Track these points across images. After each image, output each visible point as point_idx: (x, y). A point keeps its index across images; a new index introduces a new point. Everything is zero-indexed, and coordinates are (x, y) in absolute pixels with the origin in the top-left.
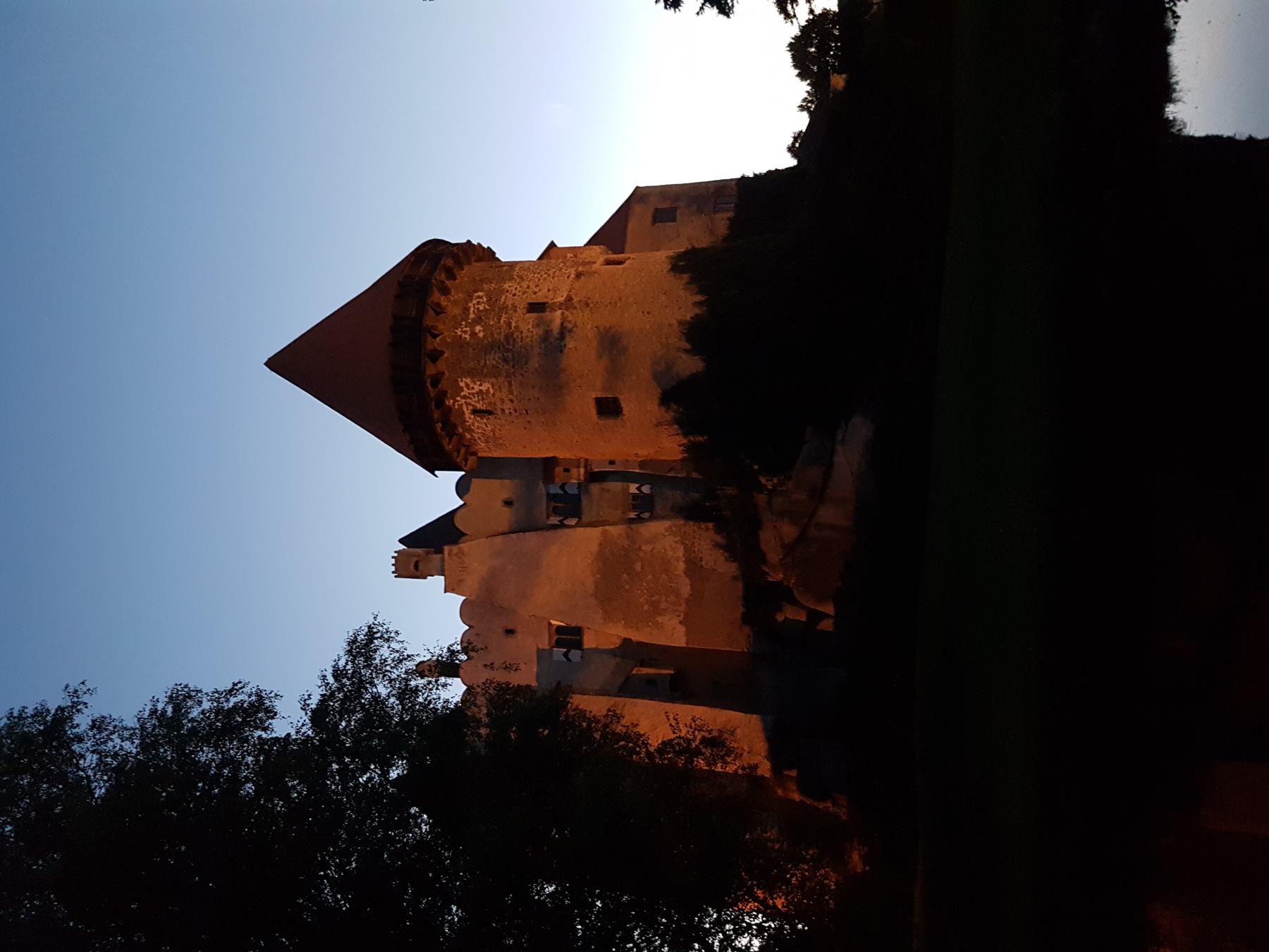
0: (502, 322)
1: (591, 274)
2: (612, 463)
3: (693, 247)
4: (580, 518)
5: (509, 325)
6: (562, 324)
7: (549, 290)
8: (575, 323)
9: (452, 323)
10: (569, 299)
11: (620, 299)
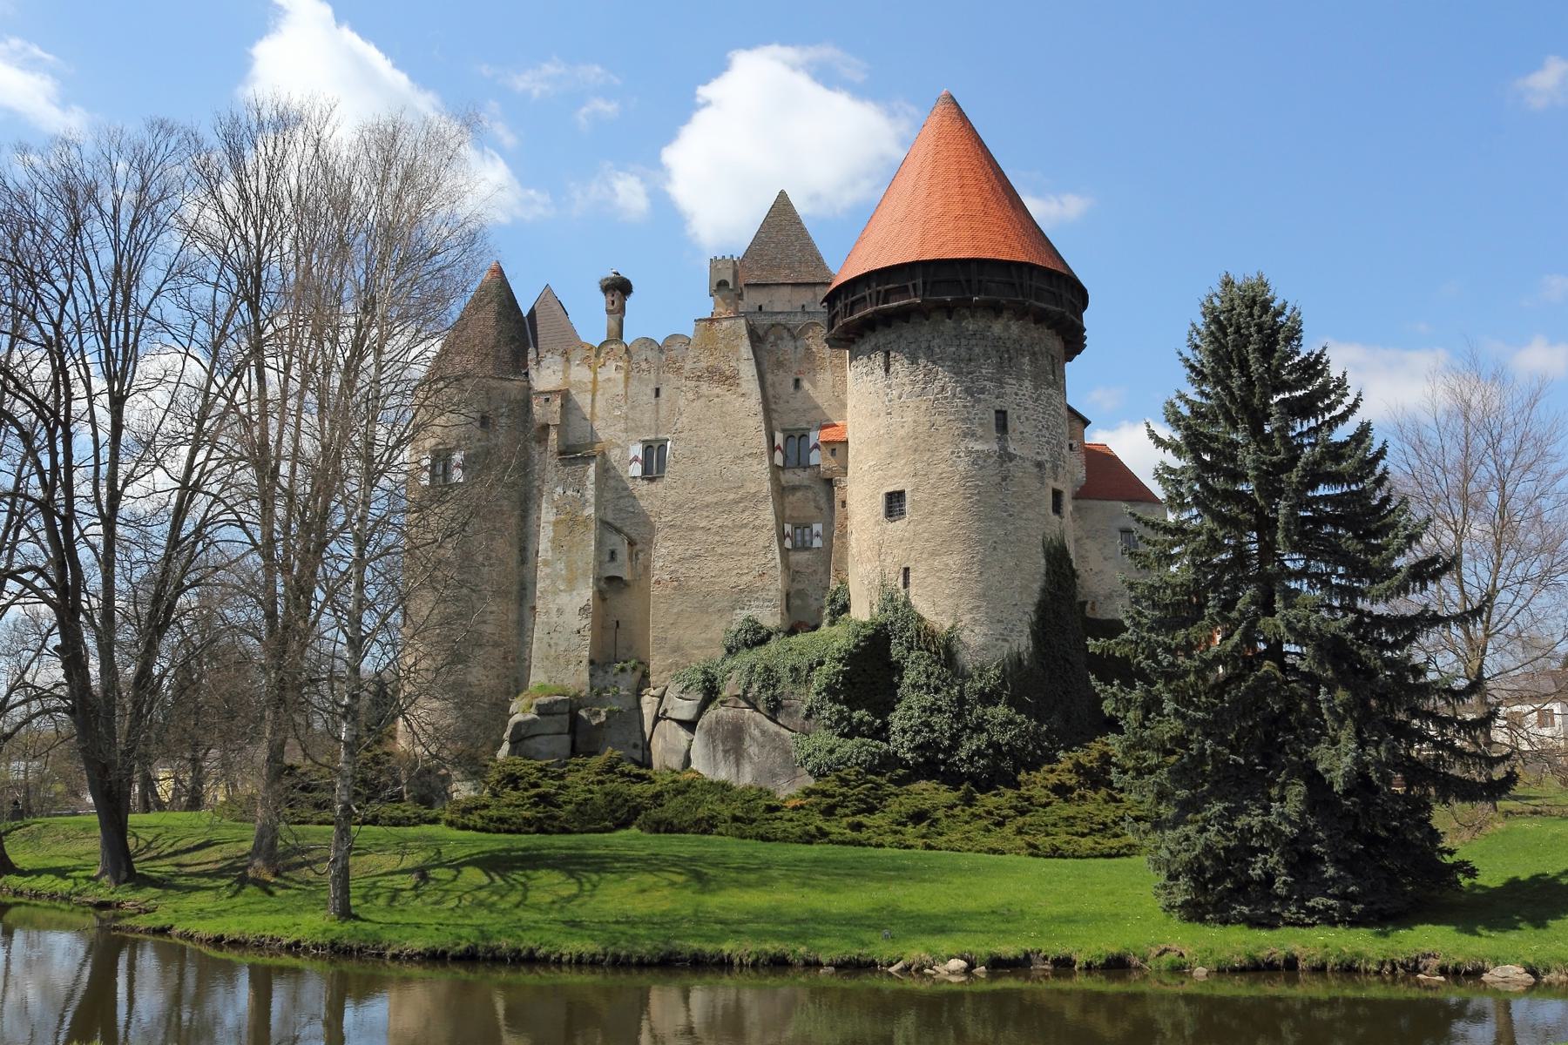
1: (1041, 479)
2: (844, 504)
7: (1022, 433)
10: (1011, 457)
11: (1011, 515)
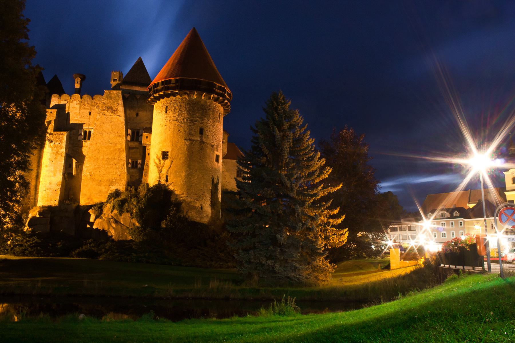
0: (197, 118)
2: (149, 154)
3: (103, 229)
4: (130, 141)
5: (196, 121)
6: (195, 140)
8: (195, 145)
9: (198, 101)
